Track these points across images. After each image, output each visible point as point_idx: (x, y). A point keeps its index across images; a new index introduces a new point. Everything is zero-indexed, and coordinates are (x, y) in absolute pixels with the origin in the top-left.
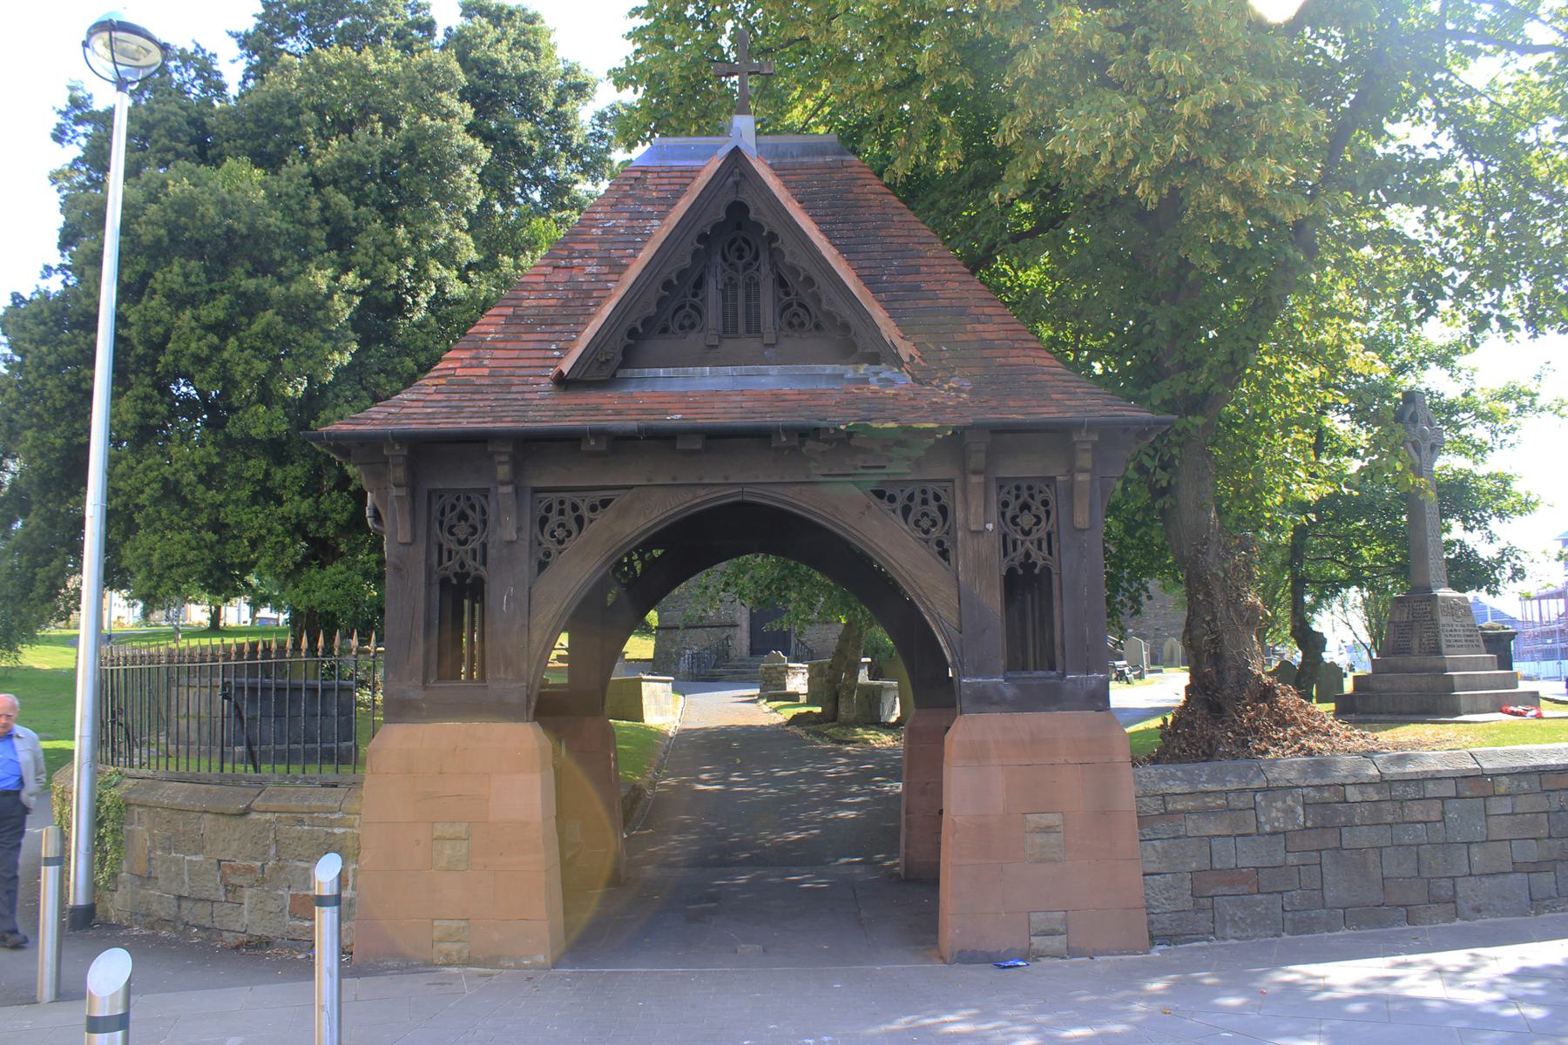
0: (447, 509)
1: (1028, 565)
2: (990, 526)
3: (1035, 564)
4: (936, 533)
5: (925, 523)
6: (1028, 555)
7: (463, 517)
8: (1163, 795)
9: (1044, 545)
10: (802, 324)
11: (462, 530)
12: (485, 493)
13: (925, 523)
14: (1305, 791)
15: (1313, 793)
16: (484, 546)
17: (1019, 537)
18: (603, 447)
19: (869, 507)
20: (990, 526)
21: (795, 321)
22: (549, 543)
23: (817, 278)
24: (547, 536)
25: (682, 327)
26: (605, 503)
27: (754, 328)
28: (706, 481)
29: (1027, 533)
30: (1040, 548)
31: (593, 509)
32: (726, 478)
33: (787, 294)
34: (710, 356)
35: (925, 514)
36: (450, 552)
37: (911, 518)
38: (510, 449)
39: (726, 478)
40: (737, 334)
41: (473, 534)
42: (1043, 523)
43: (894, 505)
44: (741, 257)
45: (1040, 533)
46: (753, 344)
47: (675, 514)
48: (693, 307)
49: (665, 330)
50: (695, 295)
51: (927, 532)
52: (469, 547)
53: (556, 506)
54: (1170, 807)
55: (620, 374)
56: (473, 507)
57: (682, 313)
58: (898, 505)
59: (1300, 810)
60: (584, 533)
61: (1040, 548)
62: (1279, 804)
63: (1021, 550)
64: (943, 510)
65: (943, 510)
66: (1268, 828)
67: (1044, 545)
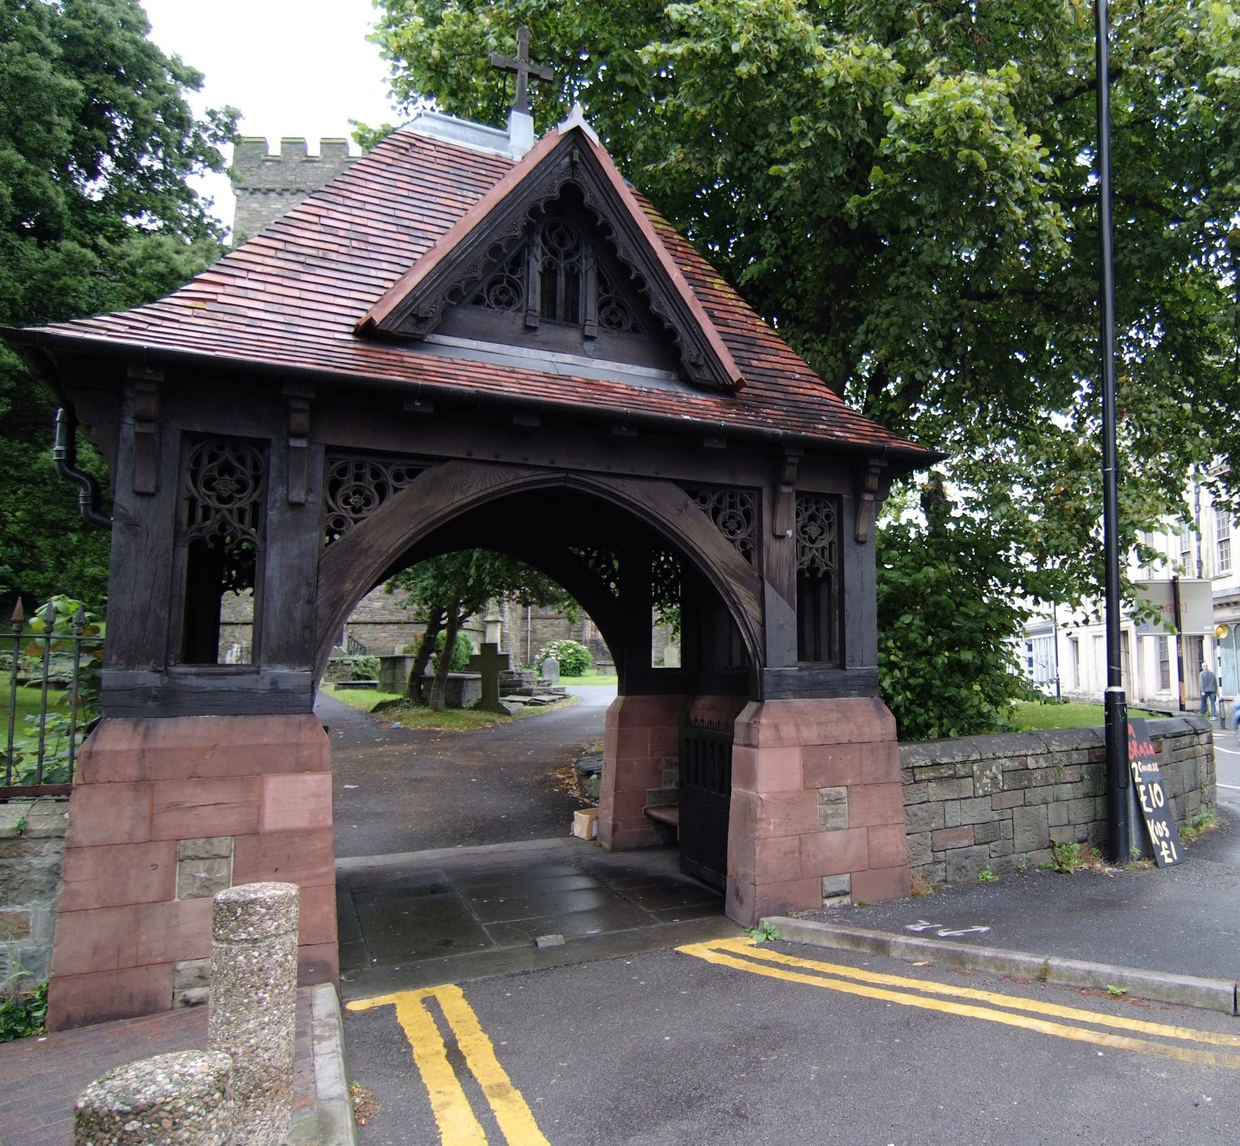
0: (205, 459)
1: (813, 569)
2: (790, 533)
3: (818, 569)
4: (741, 535)
5: (732, 524)
6: (813, 560)
7: (227, 469)
8: (913, 768)
9: (827, 553)
10: (619, 324)
11: (226, 485)
12: (263, 445)
13: (732, 524)
14: (1003, 761)
15: (1007, 763)
16: (256, 506)
17: (213, 503)
18: (429, 409)
19: (686, 505)
20: (790, 533)
21: (504, 298)
22: (345, 512)
23: (651, 284)
24: (340, 503)
25: (498, 302)
26: (413, 474)
27: (572, 318)
28: (531, 462)
29: (813, 541)
30: (241, 521)
31: (398, 477)
32: (497, 456)
33: (606, 291)
34: (527, 335)
35: (731, 517)
36: (206, 509)
37: (720, 520)
38: (312, 396)
39: (497, 456)
40: (557, 317)
41: (239, 491)
42: (248, 492)
43: (706, 506)
44: (562, 244)
45: (244, 502)
46: (573, 336)
47: (494, 493)
48: (511, 283)
49: (478, 301)
50: (512, 272)
51: (732, 533)
52: (235, 505)
53: (352, 470)
54: (918, 777)
55: (430, 338)
56: (241, 460)
57: (498, 288)
58: (710, 506)
59: (1000, 777)
60: (386, 504)
61: (241, 521)
62: (988, 773)
63: (214, 519)
64: (747, 514)
65: (747, 514)
66: (981, 792)
67: (827, 553)
